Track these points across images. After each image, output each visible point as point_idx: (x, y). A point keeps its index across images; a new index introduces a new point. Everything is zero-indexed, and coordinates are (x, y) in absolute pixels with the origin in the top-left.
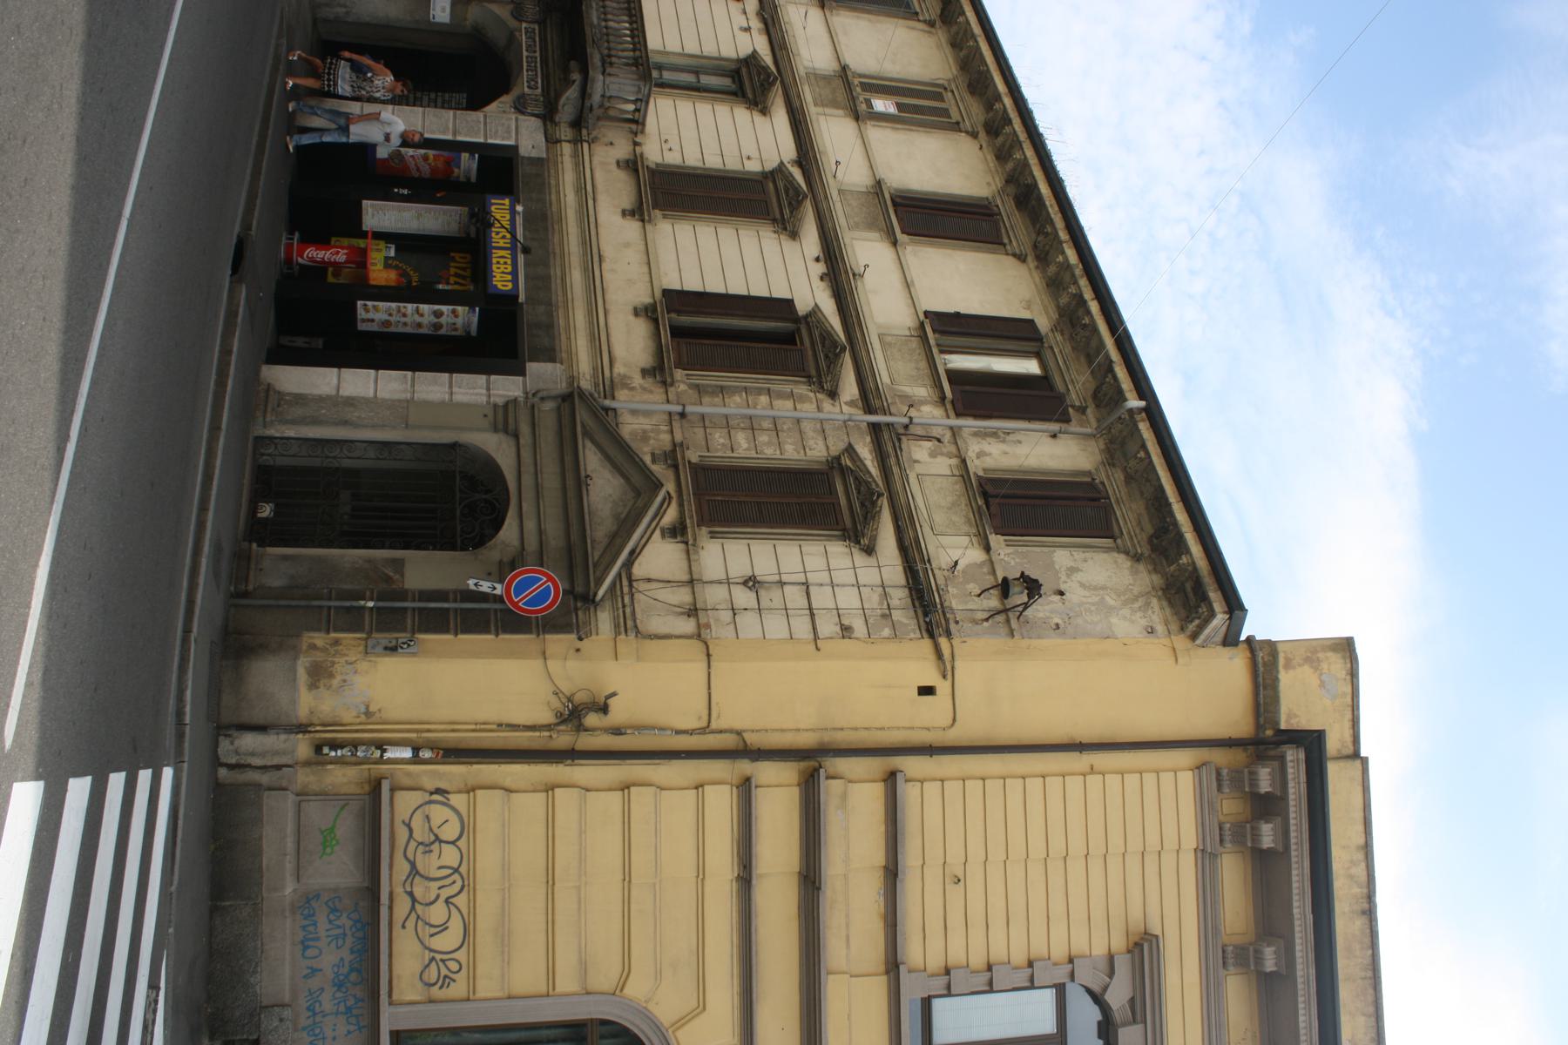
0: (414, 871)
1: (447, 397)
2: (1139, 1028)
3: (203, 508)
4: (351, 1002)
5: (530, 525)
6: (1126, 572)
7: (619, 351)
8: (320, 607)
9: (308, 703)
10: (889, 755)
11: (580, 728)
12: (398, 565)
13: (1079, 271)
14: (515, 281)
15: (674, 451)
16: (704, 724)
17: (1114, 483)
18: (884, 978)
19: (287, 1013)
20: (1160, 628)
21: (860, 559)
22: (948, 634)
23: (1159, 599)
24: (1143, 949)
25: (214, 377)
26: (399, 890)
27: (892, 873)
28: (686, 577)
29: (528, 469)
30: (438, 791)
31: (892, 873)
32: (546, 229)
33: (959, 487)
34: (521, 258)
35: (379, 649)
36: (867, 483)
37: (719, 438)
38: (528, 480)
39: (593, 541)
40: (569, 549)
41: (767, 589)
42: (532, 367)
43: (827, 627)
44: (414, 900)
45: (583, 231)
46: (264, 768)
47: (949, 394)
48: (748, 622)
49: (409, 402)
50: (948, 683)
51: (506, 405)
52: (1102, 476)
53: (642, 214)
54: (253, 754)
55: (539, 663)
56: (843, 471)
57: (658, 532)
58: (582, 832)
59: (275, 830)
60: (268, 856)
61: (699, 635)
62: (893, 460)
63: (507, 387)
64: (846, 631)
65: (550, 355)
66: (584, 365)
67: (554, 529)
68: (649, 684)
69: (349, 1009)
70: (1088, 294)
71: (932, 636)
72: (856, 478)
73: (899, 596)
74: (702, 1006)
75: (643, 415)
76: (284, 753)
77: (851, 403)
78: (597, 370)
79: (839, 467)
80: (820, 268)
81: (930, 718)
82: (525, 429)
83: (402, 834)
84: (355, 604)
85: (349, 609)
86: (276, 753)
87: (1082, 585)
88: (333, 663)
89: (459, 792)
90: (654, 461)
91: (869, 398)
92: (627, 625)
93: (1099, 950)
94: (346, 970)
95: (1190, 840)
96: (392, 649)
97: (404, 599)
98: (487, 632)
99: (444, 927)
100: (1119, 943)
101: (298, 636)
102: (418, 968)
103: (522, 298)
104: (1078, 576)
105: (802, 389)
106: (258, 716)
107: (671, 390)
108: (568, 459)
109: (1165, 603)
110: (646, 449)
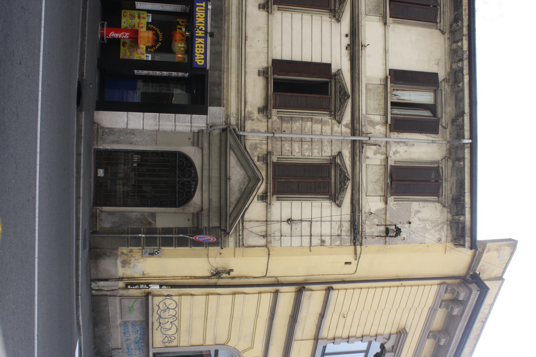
0: (160, 317)
1: (173, 128)
2: (393, 354)
3: (77, 239)
4: (140, 346)
5: (206, 196)
6: (439, 212)
7: (249, 98)
8: (125, 237)
9: (121, 272)
10: (329, 286)
11: (219, 278)
12: (153, 215)
13: (466, 56)
14: (205, 59)
15: (267, 155)
16: (264, 275)
17: (447, 171)
18: (313, 341)
19: (120, 351)
20: (444, 239)
21: (334, 207)
22: (361, 245)
23: (448, 225)
24: (402, 334)
25: (75, 170)
26: (155, 322)
27: (322, 316)
28: (264, 219)
29: (206, 167)
30: (168, 295)
31: (322, 316)
32: (222, 21)
33: (382, 171)
34: (209, 39)
35: (147, 254)
36: (344, 172)
37: (287, 147)
38: (206, 173)
39: (230, 203)
40: (220, 208)
41: (295, 224)
42: (211, 109)
43: (316, 241)
44: (160, 323)
45: (239, 22)
46: (108, 291)
47: (389, 122)
48: (286, 241)
49: (158, 131)
50: (356, 262)
51: (198, 132)
52: (442, 165)
53: (268, 8)
54: (104, 287)
55: (206, 259)
56: (336, 165)
57: (256, 197)
58: (217, 306)
59: (114, 307)
60: (111, 314)
61: (266, 246)
62: (357, 158)
63: (199, 122)
64: (323, 242)
65: (218, 102)
66: (233, 109)
67: (215, 197)
68: (245, 263)
69: (139, 348)
70: (466, 71)
71: (355, 245)
72: (340, 170)
73: (347, 226)
74: (252, 347)
75: (256, 135)
76: (115, 286)
77: (346, 126)
78: (239, 111)
79: (334, 162)
80: (346, 41)
81: (347, 271)
82: (206, 145)
83: (156, 308)
84: (137, 235)
85: (135, 237)
86: (112, 286)
87: (419, 219)
88: (130, 260)
89: (176, 296)
90: (258, 161)
91: (355, 128)
92: (240, 243)
93: (387, 332)
94: (138, 339)
95: (430, 304)
96: (152, 254)
97: (156, 233)
98: (187, 246)
99: (170, 329)
100: (394, 330)
101: (117, 249)
102: (162, 339)
103: (208, 68)
104: (419, 215)
105: (327, 118)
106: (105, 277)
107: (270, 121)
108: (223, 163)
109: (449, 228)
110: (256, 154)
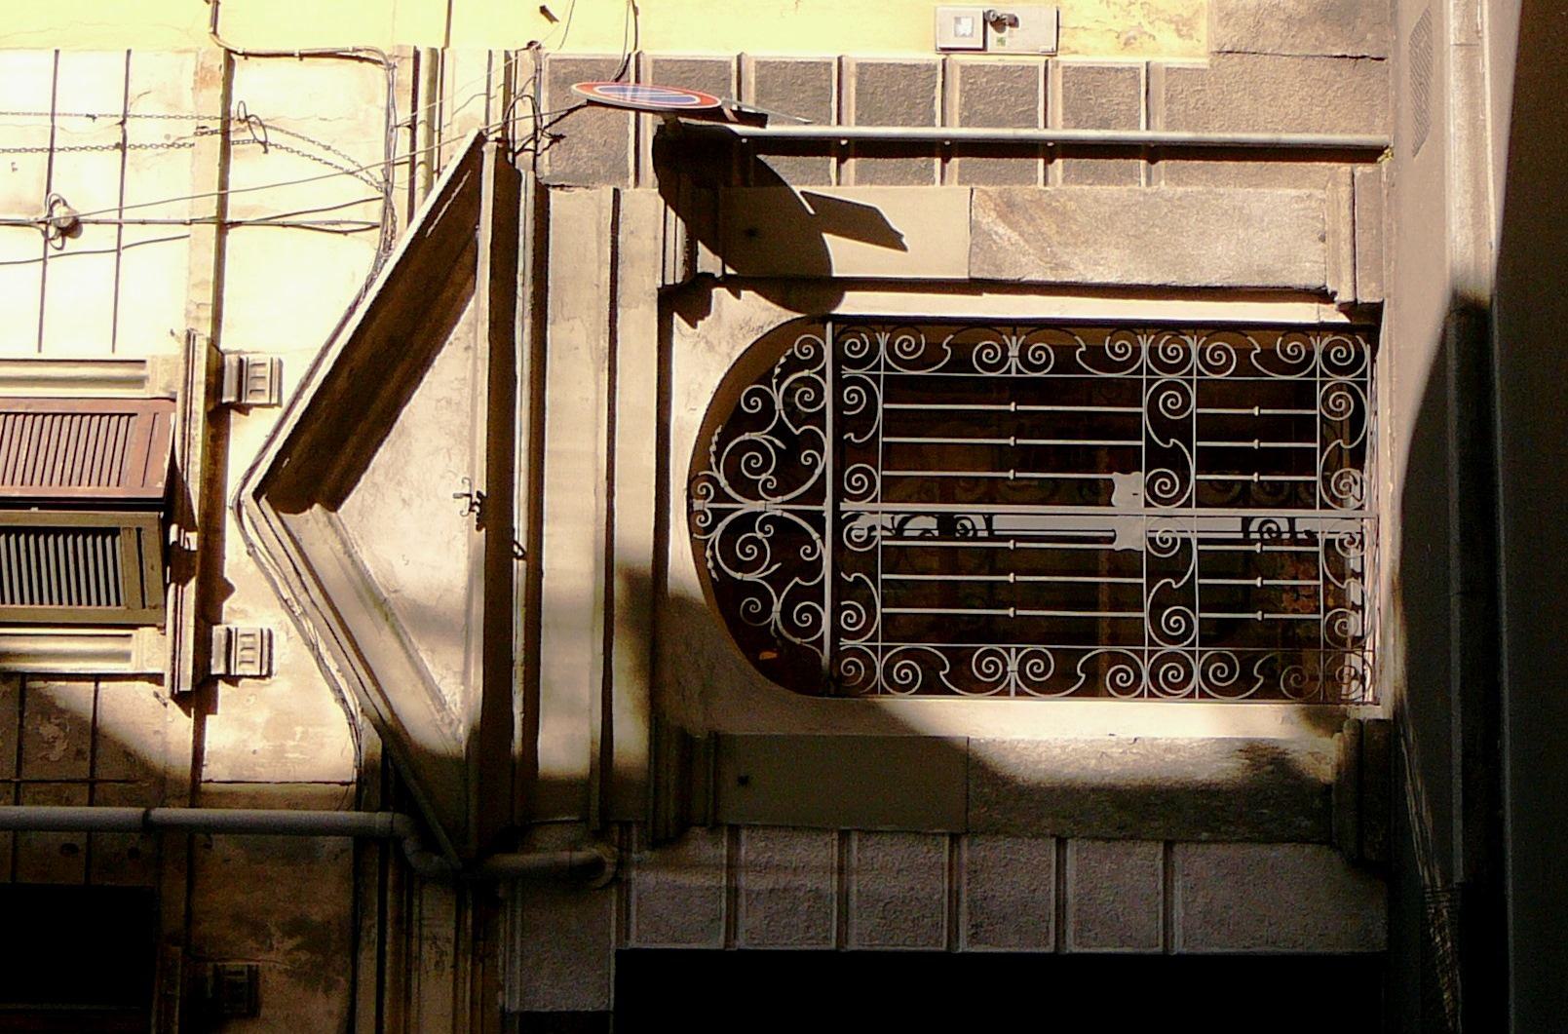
48: (91, 87)
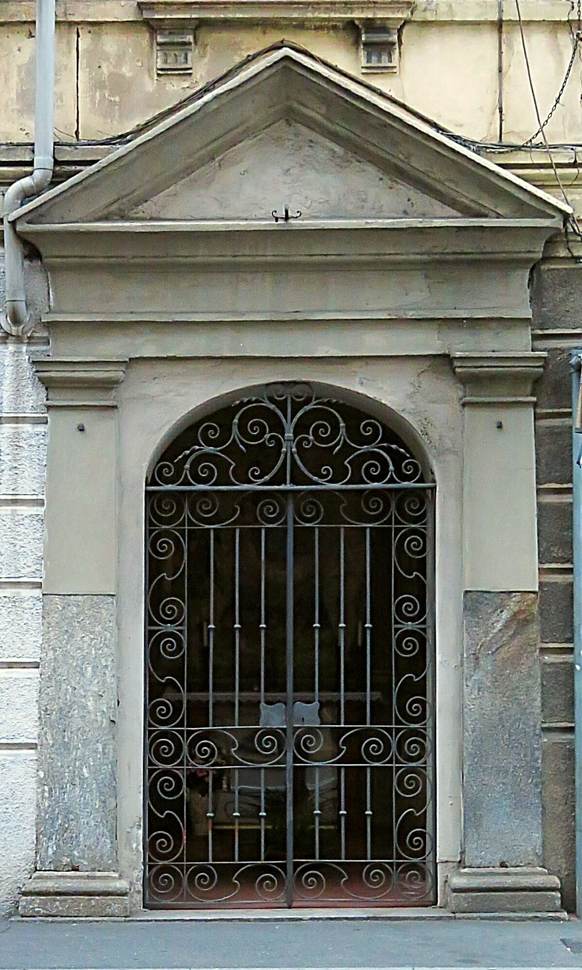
5: (374, 343)
12: (475, 602)
51: (48, 384)
67: (379, 298)
90: (185, 73)
108: (202, 254)
110: (150, 84)
